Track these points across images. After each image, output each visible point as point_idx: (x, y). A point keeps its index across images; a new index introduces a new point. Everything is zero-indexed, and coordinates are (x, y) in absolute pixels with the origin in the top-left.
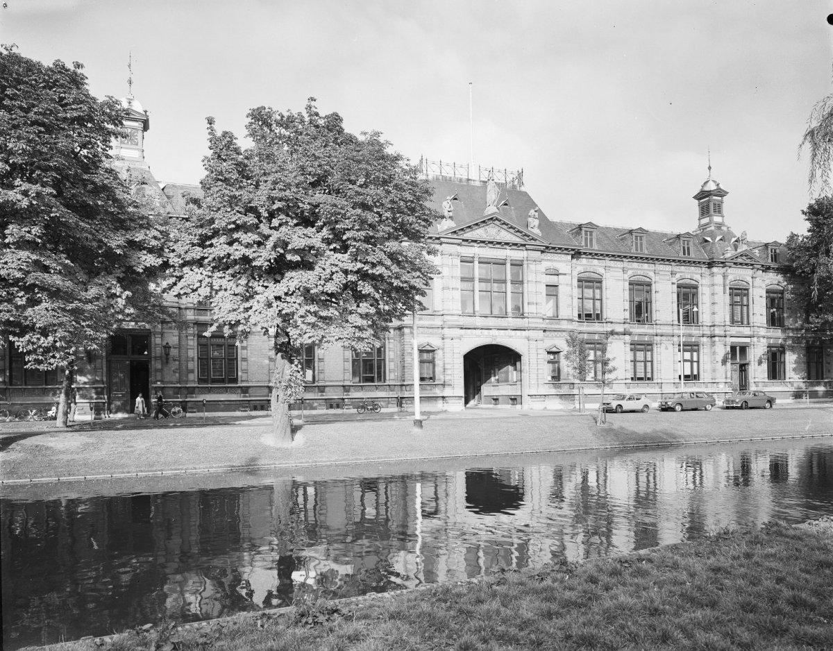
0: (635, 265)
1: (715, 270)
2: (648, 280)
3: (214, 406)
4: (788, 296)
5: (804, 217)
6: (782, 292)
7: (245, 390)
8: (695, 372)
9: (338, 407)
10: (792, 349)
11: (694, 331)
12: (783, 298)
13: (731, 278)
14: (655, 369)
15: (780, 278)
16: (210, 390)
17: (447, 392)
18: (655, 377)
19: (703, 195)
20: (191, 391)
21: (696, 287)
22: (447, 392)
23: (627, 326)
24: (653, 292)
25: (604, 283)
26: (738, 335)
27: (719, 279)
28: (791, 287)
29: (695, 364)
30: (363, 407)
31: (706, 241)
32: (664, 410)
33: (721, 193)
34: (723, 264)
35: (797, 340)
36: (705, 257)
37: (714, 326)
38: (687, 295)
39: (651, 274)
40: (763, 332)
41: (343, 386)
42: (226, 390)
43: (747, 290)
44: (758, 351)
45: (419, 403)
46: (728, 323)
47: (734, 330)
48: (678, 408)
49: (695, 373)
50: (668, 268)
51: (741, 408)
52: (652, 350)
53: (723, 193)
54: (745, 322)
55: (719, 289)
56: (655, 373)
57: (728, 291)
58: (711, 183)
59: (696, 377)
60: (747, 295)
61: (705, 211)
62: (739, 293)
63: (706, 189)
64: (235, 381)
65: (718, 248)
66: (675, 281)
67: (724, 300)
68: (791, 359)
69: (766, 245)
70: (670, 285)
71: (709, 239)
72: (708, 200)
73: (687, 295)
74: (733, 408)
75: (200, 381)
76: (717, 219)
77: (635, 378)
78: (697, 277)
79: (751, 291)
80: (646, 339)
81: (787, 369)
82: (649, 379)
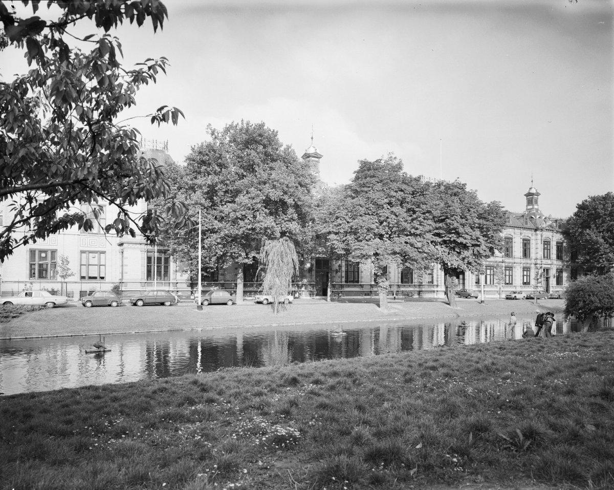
0: (525, 231)
1: (538, 232)
2: (511, 236)
3: (349, 293)
4: (565, 244)
5: (474, 190)
6: (562, 243)
7: (362, 286)
8: (528, 281)
9: (368, 295)
10: (566, 270)
11: (528, 261)
12: (562, 246)
13: (544, 236)
14: (513, 279)
15: (561, 236)
16: (349, 286)
17: (439, 289)
18: (513, 283)
19: (529, 195)
20: (342, 286)
21: (529, 240)
22: (439, 289)
23: (503, 258)
24: (531, 244)
25: (513, 240)
26: (546, 263)
27: (539, 237)
28: (565, 241)
29: (528, 277)
30: (408, 295)
31: (532, 218)
32: (507, 298)
33: (538, 194)
34: (542, 230)
35: (567, 266)
36: (533, 226)
37: (537, 259)
38: (526, 244)
39: (513, 234)
40: (555, 262)
41: (371, 285)
42: (355, 286)
43: (550, 242)
44: (553, 272)
45: (242, 293)
46: (543, 258)
47: (545, 261)
48: (114, 304)
49: (528, 281)
50: (519, 231)
51: (557, 298)
52: (512, 270)
53: (319, 156)
54: (548, 257)
55: (539, 242)
56: (513, 281)
57: (543, 242)
58: (312, 148)
59: (529, 283)
60: (550, 244)
61: (530, 202)
62: (547, 243)
63: (531, 192)
64: (358, 282)
65: (538, 222)
66: (522, 237)
67: (541, 246)
68: (565, 275)
69: (556, 221)
70: (520, 240)
71: (533, 216)
72: (531, 198)
73: (526, 244)
74: (552, 298)
75: (346, 281)
76: (536, 207)
77: (524, 283)
78: (530, 235)
79: (551, 243)
80: (510, 265)
81: (563, 281)
82: (102, 278)
